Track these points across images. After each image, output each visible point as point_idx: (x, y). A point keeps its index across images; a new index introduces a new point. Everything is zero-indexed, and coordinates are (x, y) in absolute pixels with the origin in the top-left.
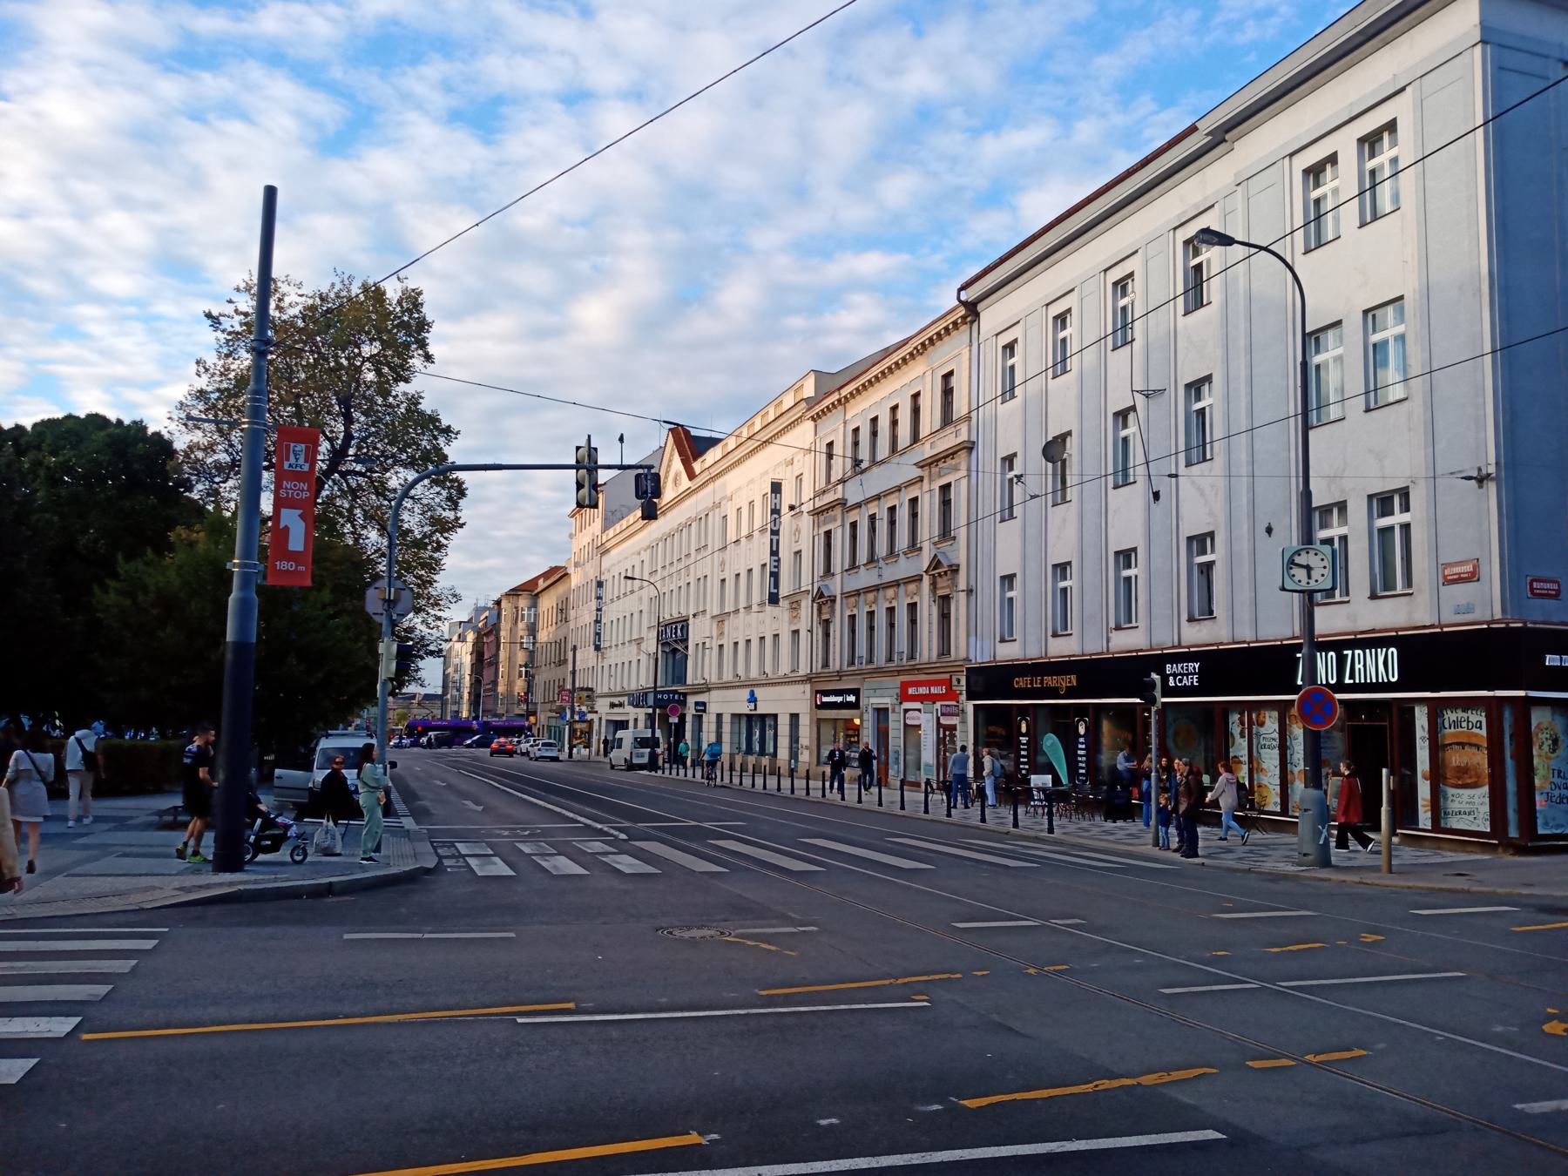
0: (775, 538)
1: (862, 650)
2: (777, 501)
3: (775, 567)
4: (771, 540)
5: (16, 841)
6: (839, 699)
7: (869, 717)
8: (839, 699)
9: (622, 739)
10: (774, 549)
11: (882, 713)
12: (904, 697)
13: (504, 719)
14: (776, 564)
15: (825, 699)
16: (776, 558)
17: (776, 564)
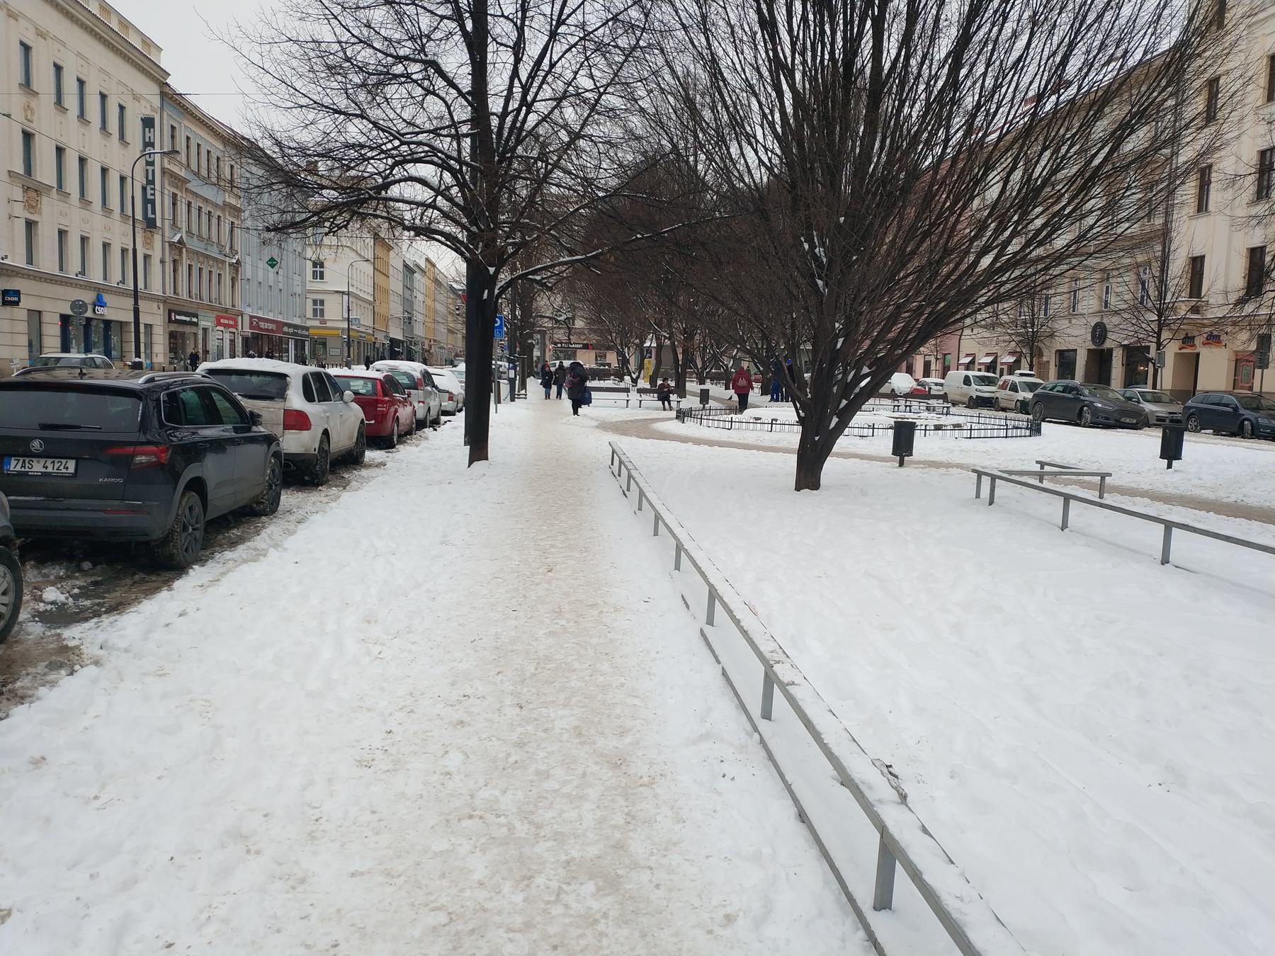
0: (150, 168)
1: (195, 290)
2: (147, 135)
3: (152, 195)
4: (147, 170)
5: (186, 486)
6: (188, 319)
7: (200, 332)
8: (188, 319)
9: (1203, 257)
10: (150, 178)
11: (205, 330)
12: (219, 324)
13: (933, 359)
14: (153, 192)
15: (178, 317)
16: (152, 186)
17: (153, 192)
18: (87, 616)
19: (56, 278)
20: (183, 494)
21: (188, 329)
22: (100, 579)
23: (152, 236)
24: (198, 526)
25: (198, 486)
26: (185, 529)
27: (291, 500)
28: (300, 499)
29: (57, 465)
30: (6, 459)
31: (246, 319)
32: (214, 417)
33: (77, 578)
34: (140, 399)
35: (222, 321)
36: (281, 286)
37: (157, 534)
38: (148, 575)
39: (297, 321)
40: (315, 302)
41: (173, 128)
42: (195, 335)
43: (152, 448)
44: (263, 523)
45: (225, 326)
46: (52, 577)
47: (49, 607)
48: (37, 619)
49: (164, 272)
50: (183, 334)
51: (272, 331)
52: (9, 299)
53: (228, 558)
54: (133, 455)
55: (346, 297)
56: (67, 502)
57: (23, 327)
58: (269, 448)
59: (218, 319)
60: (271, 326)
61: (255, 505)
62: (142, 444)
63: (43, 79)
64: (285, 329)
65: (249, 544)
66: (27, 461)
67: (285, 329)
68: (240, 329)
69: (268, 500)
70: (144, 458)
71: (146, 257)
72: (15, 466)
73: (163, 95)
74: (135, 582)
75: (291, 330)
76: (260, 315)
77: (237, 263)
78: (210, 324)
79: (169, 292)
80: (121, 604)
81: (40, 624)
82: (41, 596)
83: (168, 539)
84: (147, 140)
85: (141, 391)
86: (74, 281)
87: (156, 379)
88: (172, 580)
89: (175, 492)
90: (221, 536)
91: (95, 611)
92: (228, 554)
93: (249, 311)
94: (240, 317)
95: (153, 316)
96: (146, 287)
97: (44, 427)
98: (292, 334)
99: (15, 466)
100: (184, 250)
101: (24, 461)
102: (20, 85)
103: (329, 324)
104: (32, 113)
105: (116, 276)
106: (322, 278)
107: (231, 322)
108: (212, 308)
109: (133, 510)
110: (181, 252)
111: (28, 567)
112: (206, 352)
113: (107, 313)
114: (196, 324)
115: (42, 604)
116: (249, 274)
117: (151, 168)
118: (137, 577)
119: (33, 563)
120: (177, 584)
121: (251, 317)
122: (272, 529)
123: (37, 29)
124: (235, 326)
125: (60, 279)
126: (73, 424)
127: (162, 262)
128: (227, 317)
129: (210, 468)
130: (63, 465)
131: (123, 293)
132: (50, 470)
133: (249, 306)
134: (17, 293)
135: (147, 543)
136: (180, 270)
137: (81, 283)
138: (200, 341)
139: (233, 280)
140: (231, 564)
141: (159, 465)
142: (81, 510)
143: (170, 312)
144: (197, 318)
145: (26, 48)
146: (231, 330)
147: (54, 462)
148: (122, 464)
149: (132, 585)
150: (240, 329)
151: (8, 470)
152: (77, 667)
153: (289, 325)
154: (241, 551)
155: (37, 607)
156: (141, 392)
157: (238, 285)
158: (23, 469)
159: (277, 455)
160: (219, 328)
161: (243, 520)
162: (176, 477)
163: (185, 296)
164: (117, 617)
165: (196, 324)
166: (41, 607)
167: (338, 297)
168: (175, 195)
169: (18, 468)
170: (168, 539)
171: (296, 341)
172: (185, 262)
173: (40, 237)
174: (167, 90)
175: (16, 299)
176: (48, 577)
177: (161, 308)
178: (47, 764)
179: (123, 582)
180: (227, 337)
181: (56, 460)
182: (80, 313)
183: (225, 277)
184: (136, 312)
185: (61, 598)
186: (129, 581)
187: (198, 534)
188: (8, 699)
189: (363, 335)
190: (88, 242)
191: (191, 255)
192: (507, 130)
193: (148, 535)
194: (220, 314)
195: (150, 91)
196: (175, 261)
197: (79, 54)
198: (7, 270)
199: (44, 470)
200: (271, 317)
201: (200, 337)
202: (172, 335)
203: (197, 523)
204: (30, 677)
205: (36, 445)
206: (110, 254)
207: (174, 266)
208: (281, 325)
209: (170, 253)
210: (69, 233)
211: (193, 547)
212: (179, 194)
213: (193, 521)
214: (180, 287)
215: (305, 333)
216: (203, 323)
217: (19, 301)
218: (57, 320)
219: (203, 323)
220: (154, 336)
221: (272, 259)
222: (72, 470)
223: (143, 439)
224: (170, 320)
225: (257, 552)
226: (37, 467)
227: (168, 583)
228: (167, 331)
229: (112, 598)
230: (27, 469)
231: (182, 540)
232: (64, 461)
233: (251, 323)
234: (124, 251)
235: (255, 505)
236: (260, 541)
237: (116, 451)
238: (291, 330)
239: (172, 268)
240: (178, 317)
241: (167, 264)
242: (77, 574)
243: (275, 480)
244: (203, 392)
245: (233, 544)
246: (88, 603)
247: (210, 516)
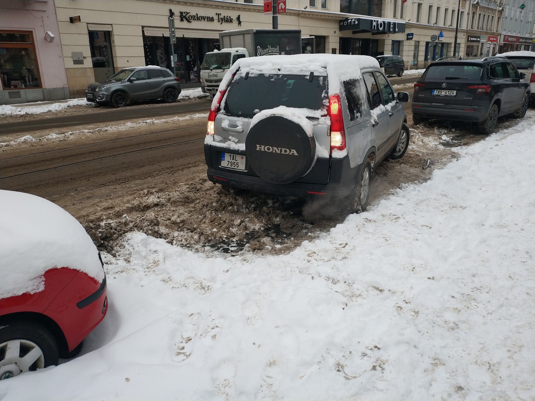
1: (480, 26)
6: (476, 39)
7: (480, 45)
8: (476, 39)
11: (482, 44)
12: (489, 40)
15: (471, 39)
18: (457, 145)
19: (426, 27)
20: (492, 106)
21: (475, 44)
22: (458, 135)
23: (466, 2)
24: (496, 118)
25: (498, 102)
26: (491, 119)
27: (529, 113)
28: (533, 113)
29: (450, 93)
30: (433, 90)
31: (502, 37)
32: (506, 74)
33: (450, 134)
34: (482, 67)
35: (491, 39)
36: (522, 18)
37: (481, 120)
38: (475, 135)
39: (527, 36)
42: (478, 46)
43: (484, 86)
44: (518, 121)
45: (492, 41)
46: (442, 133)
47: (444, 142)
48: (441, 144)
49: (468, 19)
50: (472, 46)
51: (514, 42)
52: (409, 37)
53: (506, 132)
54: (477, 89)
56: (452, 106)
57: (413, 48)
58: (526, 89)
59: (489, 38)
60: (514, 39)
61: (515, 114)
62: (481, 84)
64: (521, 40)
65: (514, 128)
66: (440, 91)
67: (521, 40)
68: (498, 42)
69: (521, 112)
70: (481, 90)
71: (462, 12)
72: (436, 93)
74: (470, 137)
75: (524, 41)
76: (509, 34)
77: (502, 10)
78: (485, 41)
79: (469, 28)
80: (467, 143)
81: (442, 146)
82: (441, 138)
83: (485, 121)
85: (482, 64)
86: (433, 27)
87: (488, 59)
88: (485, 138)
89: (490, 104)
90: (501, 125)
91: (459, 144)
92: (505, 131)
93: (504, 33)
94: (499, 36)
95: (462, 40)
96: (460, 27)
97: (447, 78)
98: (524, 43)
99: (436, 93)
100: (479, 7)
101: (439, 91)
105: (448, 23)
107: (495, 39)
108: (487, 33)
109: (475, 110)
110: (477, 8)
111: (435, 129)
112: (481, 54)
113: (443, 40)
114: (479, 41)
115: (442, 140)
116: (507, 15)
118: (471, 135)
119: (437, 127)
120: (487, 139)
121: (505, 36)
122: (522, 124)
124: (496, 41)
125: (428, 27)
126: (455, 77)
127: (468, 14)
128: (493, 36)
129: (503, 96)
130: (452, 93)
131: (451, 30)
132: (447, 94)
133: (504, 30)
134: (412, 34)
135: (477, 123)
136: (475, 17)
137: (435, 27)
138: (480, 49)
139: (499, 18)
140: (507, 134)
141: (486, 93)
142: (456, 109)
144: (480, 39)
146: (495, 43)
147: (449, 91)
148: (473, 92)
149: (470, 138)
150: (498, 42)
151: (434, 94)
152: (459, 159)
153: (523, 38)
154: (510, 130)
155: (440, 141)
156: (482, 64)
157: (501, 21)
158: (438, 94)
159: (528, 92)
160: (489, 42)
161: (509, 119)
162: (492, 98)
163: (476, 28)
164: (467, 147)
165: (479, 41)
166: (441, 141)
169: (437, 94)
170: (485, 121)
171: (525, 46)
172: (478, 12)
173: (422, 10)
175: (412, 37)
176: (441, 133)
177: (465, 35)
178: (462, 179)
179: (466, 137)
180: (492, 46)
181: (450, 91)
182: (434, 40)
183: (495, 18)
184: (456, 38)
185: (448, 139)
186: (468, 136)
187: (495, 121)
188: (440, 164)
190: (440, 9)
191: (481, 9)
193: (477, 120)
194: (489, 35)
196: (474, 13)
198: (410, 25)
199: (445, 94)
200: (514, 35)
201: (480, 47)
202: (468, 47)
203: (495, 117)
204: (446, 159)
205: (444, 85)
206: (447, 13)
207: (473, 15)
208: (518, 38)
209: (472, 9)
210: (441, 8)
211: (493, 126)
213: (494, 116)
214: (474, 25)
215: (531, 41)
216: (482, 41)
217: (413, 38)
218: (424, 44)
219: (482, 41)
220: (460, 48)
222: (455, 94)
223: (481, 83)
224: (468, 41)
225: (517, 131)
226: (443, 93)
227: (483, 138)
228: (466, 46)
229: (463, 141)
230: (440, 94)
231: (490, 123)
232: (452, 91)
233: (504, 38)
234: (453, 11)
235: (515, 114)
236: (519, 127)
237: (472, 87)
238: (524, 41)
239: (472, 16)
240: (472, 39)
241: (470, 15)
242: (450, 133)
243: (526, 103)
244: (504, 65)
245: (507, 128)
246: (456, 142)
247: (501, 115)
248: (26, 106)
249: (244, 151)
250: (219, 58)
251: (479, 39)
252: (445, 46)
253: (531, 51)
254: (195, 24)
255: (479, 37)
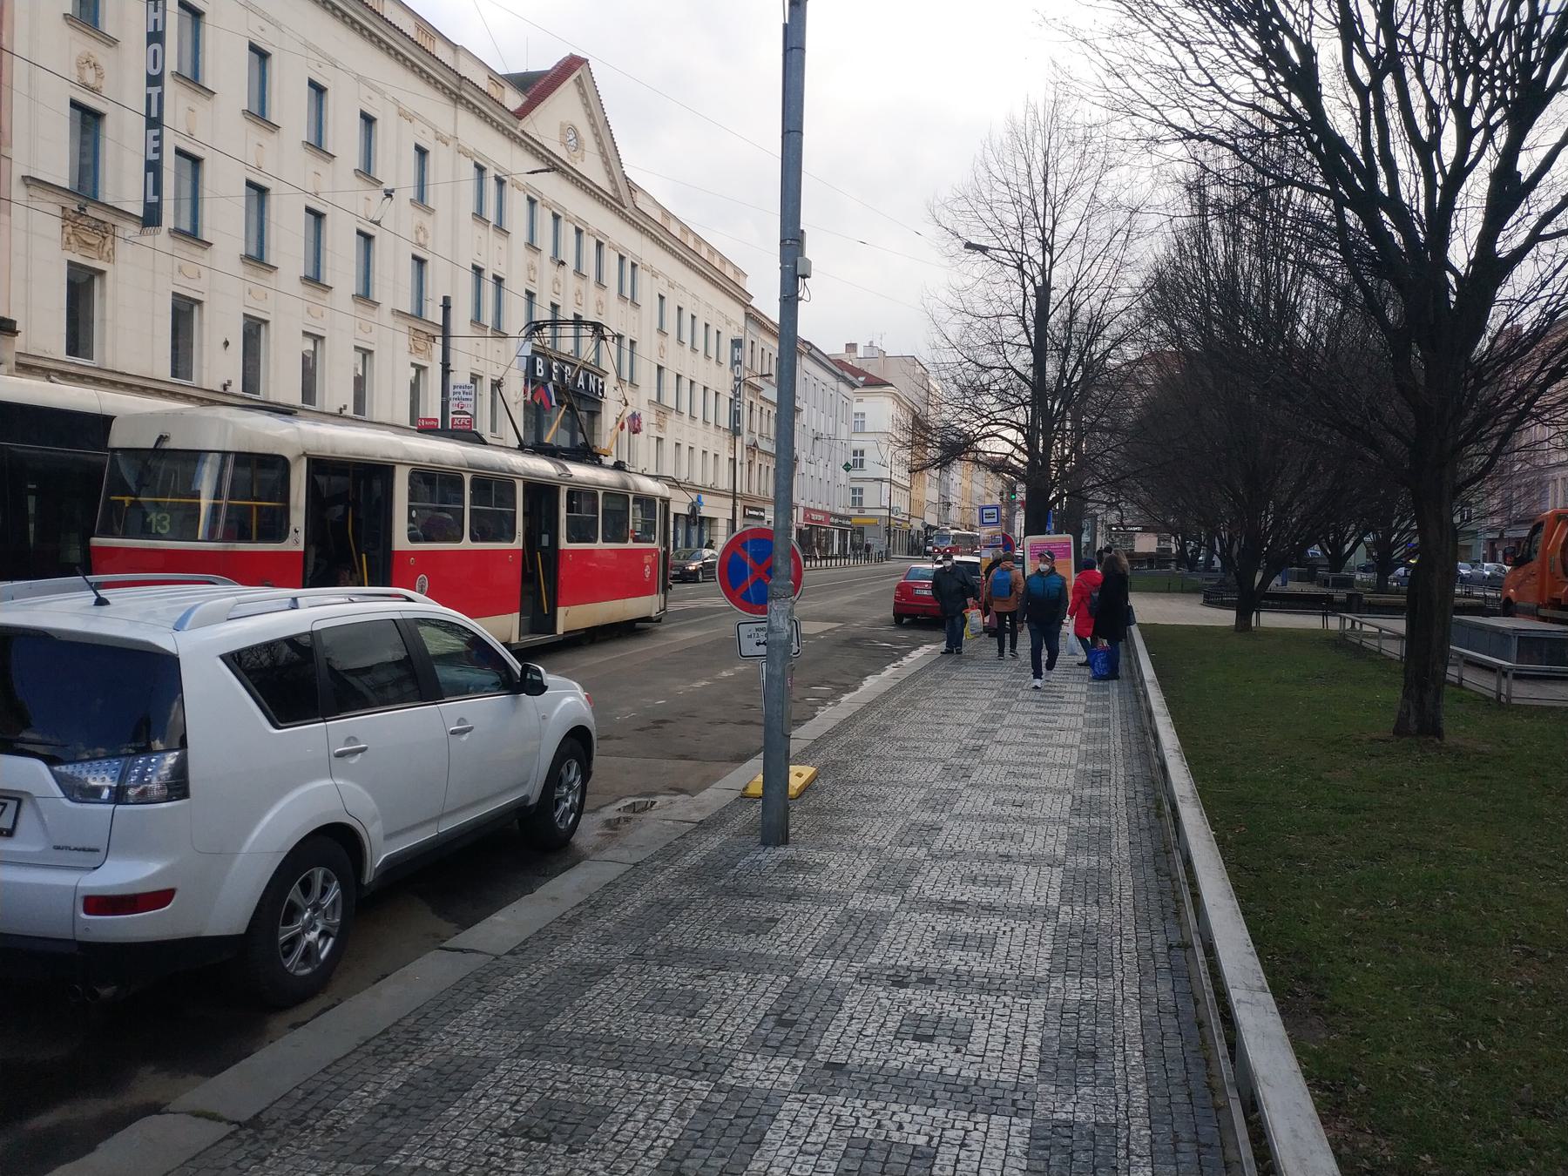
0: (155, 91)
1: (763, 488)
4: (149, 97)
6: (757, 513)
8: (757, 513)
10: (154, 114)
14: (156, 144)
15: (751, 512)
31: (801, 510)
40: (854, 490)
41: (753, 342)
55: (886, 485)
60: (820, 517)
63: (290, 103)
64: (832, 520)
67: (832, 520)
73: (747, 315)
75: (836, 521)
84: (151, 29)
93: (803, 503)
98: (837, 525)
102: (248, 113)
103: (867, 512)
104: (426, 236)
106: (861, 466)
117: (157, 89)
121: (805, 508)
123: (437, 132)
143: (745, 507)
145: (422, 152)
153: (836, 516)
167: (876, 485)
168: (751, 403)
174: (751, 311)
189: (899, 523)
192: (1155, 707)
195: (737, 313)
196: (750, 462)
197: (694, 296)
212: (755, 401)
221: (847, 464)
233: (805, 515)
238: (836, 521)
240: (751, 512)
248: (1184, 833)
249: (391, 546)
250: (1516, 588)
251: (762, 514)
252: (706, 523)
253: (199, 498)
254: (758, 414)
255: (763, 510)
